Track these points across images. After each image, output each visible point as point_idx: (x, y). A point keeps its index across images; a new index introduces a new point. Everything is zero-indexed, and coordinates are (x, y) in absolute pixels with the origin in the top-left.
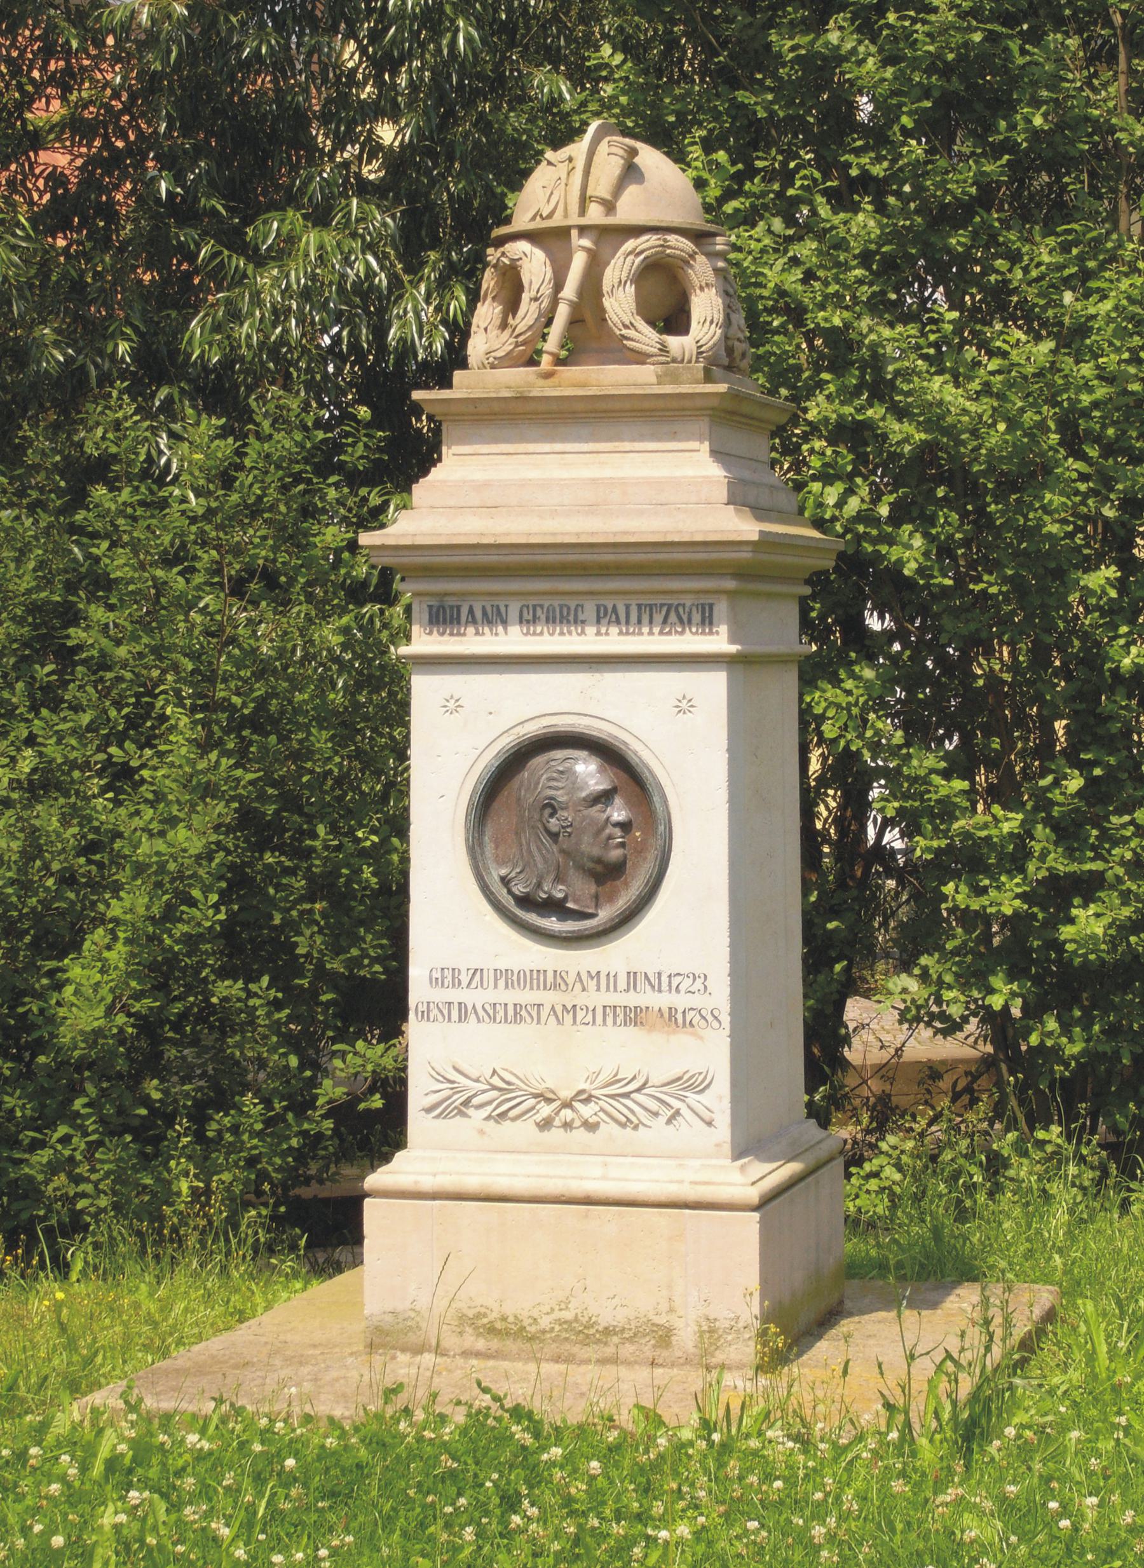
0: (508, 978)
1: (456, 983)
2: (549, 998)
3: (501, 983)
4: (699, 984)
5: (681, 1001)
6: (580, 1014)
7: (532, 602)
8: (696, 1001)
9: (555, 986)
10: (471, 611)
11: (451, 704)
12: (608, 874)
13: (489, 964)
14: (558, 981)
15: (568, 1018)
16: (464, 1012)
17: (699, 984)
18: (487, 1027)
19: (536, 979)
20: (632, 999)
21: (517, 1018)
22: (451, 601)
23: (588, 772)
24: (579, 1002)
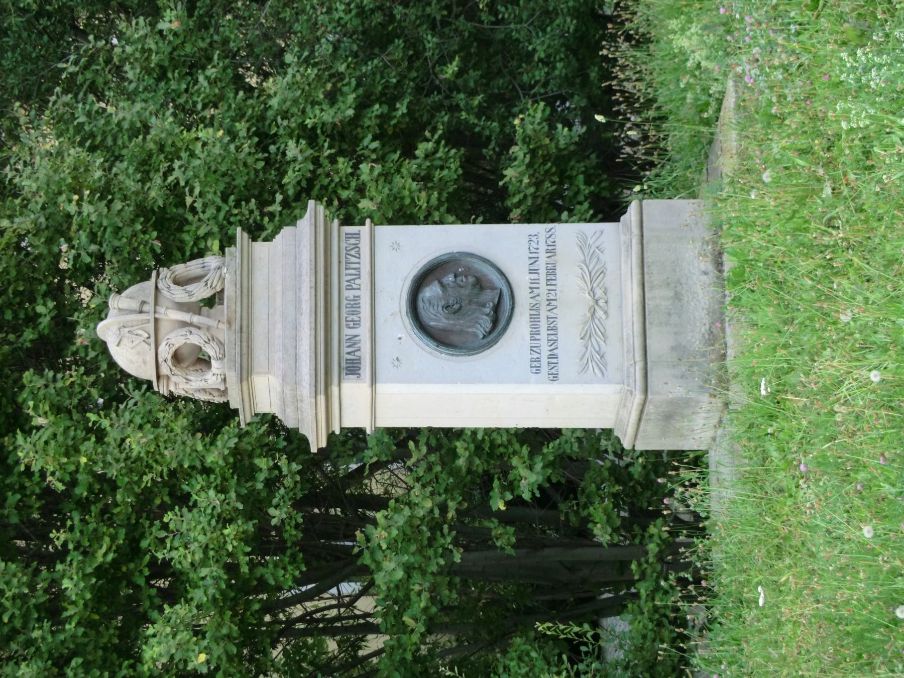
0: (534, 334)
1: (538, 360)
2: (544, 313)
3: (537, 337)
4: (534, 239)
5: (543, 247)
6: (551, 297)
7: (344, 323)
8: (542, 239)
9: (538, 309)
10: (349, 353)
11: (395, 246)
12: (480, 284)
13: (528, 343)
14: (535, 308)
15: (554, 303)
16: (552, 356)
17: (534, 239)
18: (560, 344)
19: (534, 319)
20: (543, 271)
21: (555, 329)
22: (344, 365)
23: (431, 291)
24: (545, 298)
